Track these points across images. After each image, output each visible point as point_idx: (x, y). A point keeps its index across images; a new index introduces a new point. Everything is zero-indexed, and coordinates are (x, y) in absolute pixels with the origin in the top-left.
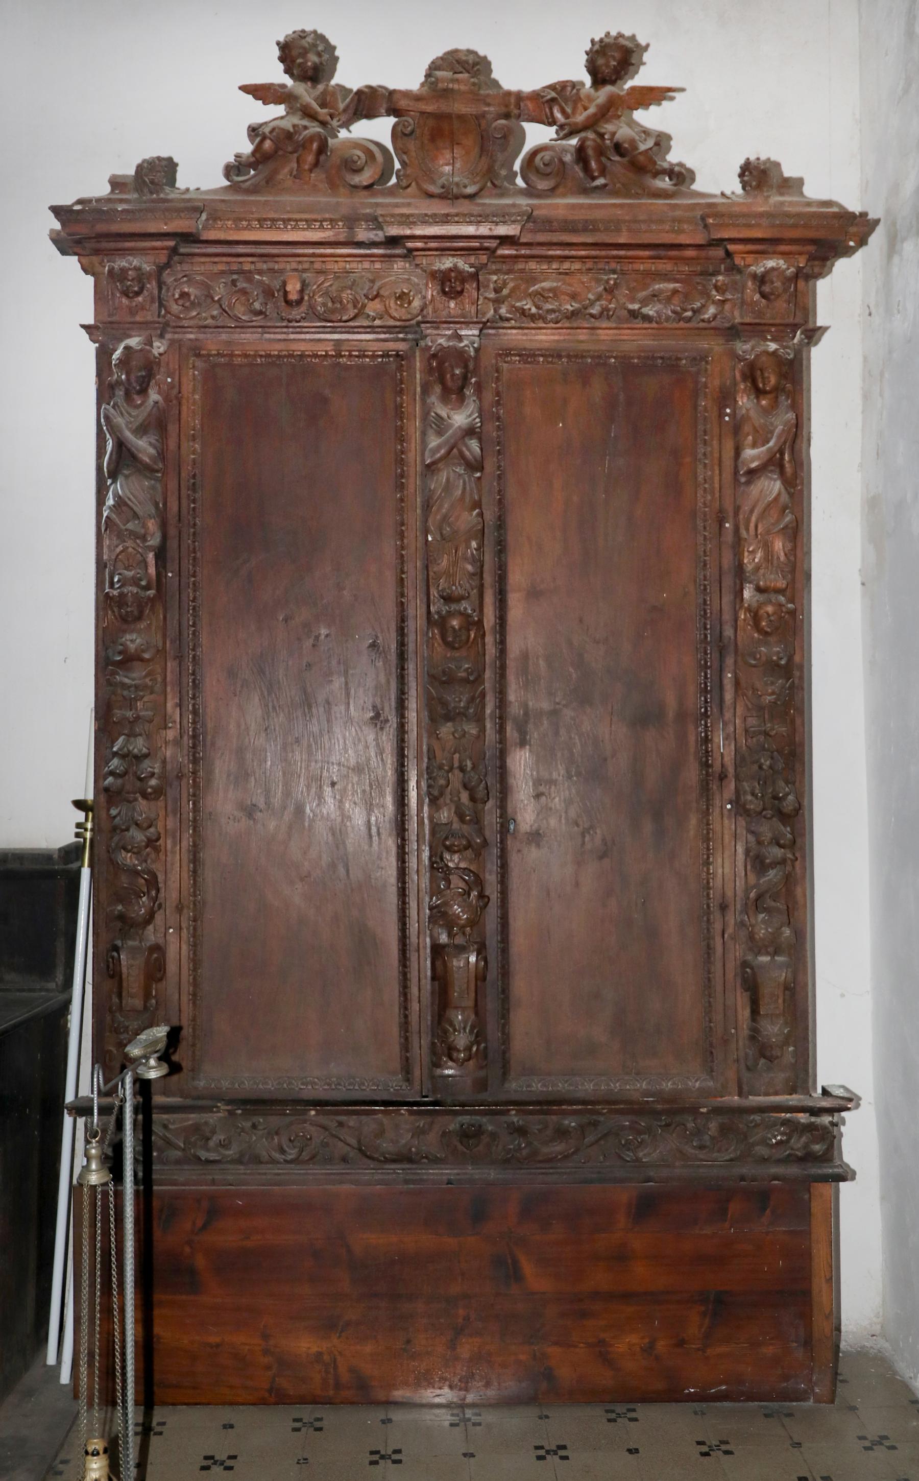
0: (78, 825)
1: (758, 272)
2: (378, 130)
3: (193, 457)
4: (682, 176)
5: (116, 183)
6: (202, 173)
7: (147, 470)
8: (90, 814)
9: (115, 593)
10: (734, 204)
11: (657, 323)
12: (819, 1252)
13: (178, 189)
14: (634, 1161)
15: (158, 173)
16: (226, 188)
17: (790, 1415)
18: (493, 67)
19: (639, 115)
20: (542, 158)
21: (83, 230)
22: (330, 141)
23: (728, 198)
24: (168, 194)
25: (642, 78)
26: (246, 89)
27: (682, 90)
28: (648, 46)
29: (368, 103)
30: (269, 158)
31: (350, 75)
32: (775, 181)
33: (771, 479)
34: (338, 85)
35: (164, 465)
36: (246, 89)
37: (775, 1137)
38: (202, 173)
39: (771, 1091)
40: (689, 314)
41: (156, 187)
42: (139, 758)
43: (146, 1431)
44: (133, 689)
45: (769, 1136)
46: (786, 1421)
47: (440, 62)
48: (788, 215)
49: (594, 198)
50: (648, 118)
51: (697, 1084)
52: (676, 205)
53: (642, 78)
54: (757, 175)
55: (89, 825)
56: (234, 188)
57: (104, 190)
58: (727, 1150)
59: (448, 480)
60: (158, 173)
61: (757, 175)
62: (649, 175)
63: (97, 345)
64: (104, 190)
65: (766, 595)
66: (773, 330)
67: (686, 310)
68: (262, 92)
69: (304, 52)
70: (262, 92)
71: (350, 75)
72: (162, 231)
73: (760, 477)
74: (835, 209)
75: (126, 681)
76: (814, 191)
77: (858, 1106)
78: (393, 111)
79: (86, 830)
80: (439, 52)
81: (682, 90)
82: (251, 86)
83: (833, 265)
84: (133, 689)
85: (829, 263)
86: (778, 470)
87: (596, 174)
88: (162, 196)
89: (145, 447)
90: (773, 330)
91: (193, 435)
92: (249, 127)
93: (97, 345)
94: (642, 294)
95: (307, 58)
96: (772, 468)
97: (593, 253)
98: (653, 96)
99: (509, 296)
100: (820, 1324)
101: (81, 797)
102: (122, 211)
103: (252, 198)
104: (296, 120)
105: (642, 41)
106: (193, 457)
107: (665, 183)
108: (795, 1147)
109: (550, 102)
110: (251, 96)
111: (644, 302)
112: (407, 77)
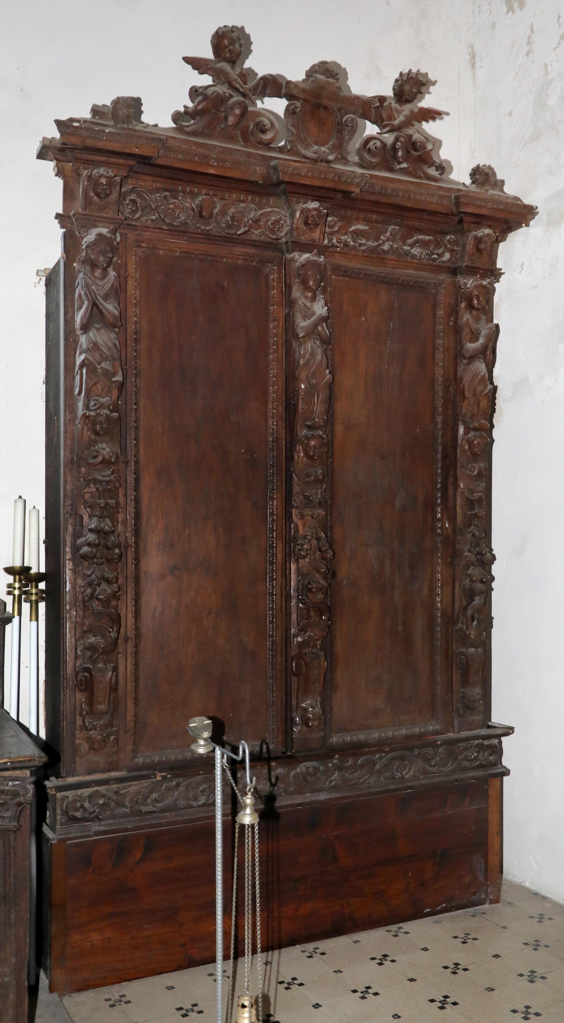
0: (9, 586)
1: (478, 235)
2: (276, 106)
3: (135, 319)
4: (443, 168)
5: (96, 111)
6: (159, 114)
7: (111, 326)
8: (17, 577)
9: (92, 413)
10: (470, 192)
11: (418, 260)
12: (493, 818)
13: (142, 123)
14: (401, 778)
15: (130, 108)
16: (174, 129)
17: (484, 913)
18: (349, 76)
19: (425, 125)
20: (375, 143)
21: (75, 141)
22: (250, 109)
23: (467, 187)
24: (135, 126)
25: (427, 102)
26: (187, 60)
27: (448, 114)
28: (436, 81)
29: (273, 85)
30: (205, 111)
31: (259, 63)
32: (493, 180)
33: (481, 362)
34: (250, 69)
35: (117, 324)
36: (187, 60)
37: (473, 755)
38: (159, 114)
39: (472, 727)
40: (435, 256)
41: (127, 120)
42: (107, 533)
43: (252, 959)
44: (104, 484)
45: (470, 754)
46: (484, 916)
47: (317, 68)
48: (501, 203)
49: (396, 175)
50: (430, 128)
51: (431, 728)
52: (441, 187)
53: (427, 102)
54: (482, 175)
55: (17, 585)
56: (180, 129)
57: (87, 115)
58: (447, 765)
59: (312, 348)
60: (130, 108)
61: (482, 175)
62: (427, 165)
63: (64, 230)
64: (87, 115)
65: (479, 432)
66: (481, 272)
67: (434, 254)
68: (197, 64)
69: (232, 42)
70: (197, 64)
71: (259, 63)
72: (134, 152)
73: (474, 361)
74: (520, 203)
75: (99, 477)
76: (510, 189)
77: (513, 732)
78: (290, 97)
79: (15, 588)
80: (316, 60)
81: (448, 114)
82: (192, 58)
83: (507, 236)
84: (104, 484)
85: (505, 235)
86: (483, 357)
87: (401, 160)
88: (130, 126)
89: (110, 307)
90: (481, 272)
91: (135, 303)
92: (191, 88)
93: (64, 230)
94: (410, 241)
95: (230, 45)
96: (480, 356)
97: (390, 211)
98: (432, 115)
99: (337, 231)
100: (493, 860)
101: (9, 565)
102: (108, 133)
103: (192, 139)
104: (222, 89)
105: (432, 77)
106: (135, 319)
107: (432, 172)
108: (481, 759)
109: (373, 109)
110: (190, 66)
111: (412, 246)
112: (296, 74)
